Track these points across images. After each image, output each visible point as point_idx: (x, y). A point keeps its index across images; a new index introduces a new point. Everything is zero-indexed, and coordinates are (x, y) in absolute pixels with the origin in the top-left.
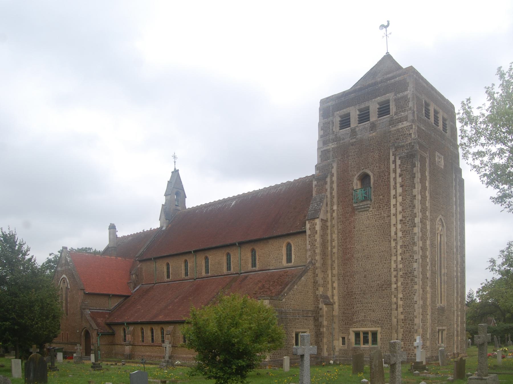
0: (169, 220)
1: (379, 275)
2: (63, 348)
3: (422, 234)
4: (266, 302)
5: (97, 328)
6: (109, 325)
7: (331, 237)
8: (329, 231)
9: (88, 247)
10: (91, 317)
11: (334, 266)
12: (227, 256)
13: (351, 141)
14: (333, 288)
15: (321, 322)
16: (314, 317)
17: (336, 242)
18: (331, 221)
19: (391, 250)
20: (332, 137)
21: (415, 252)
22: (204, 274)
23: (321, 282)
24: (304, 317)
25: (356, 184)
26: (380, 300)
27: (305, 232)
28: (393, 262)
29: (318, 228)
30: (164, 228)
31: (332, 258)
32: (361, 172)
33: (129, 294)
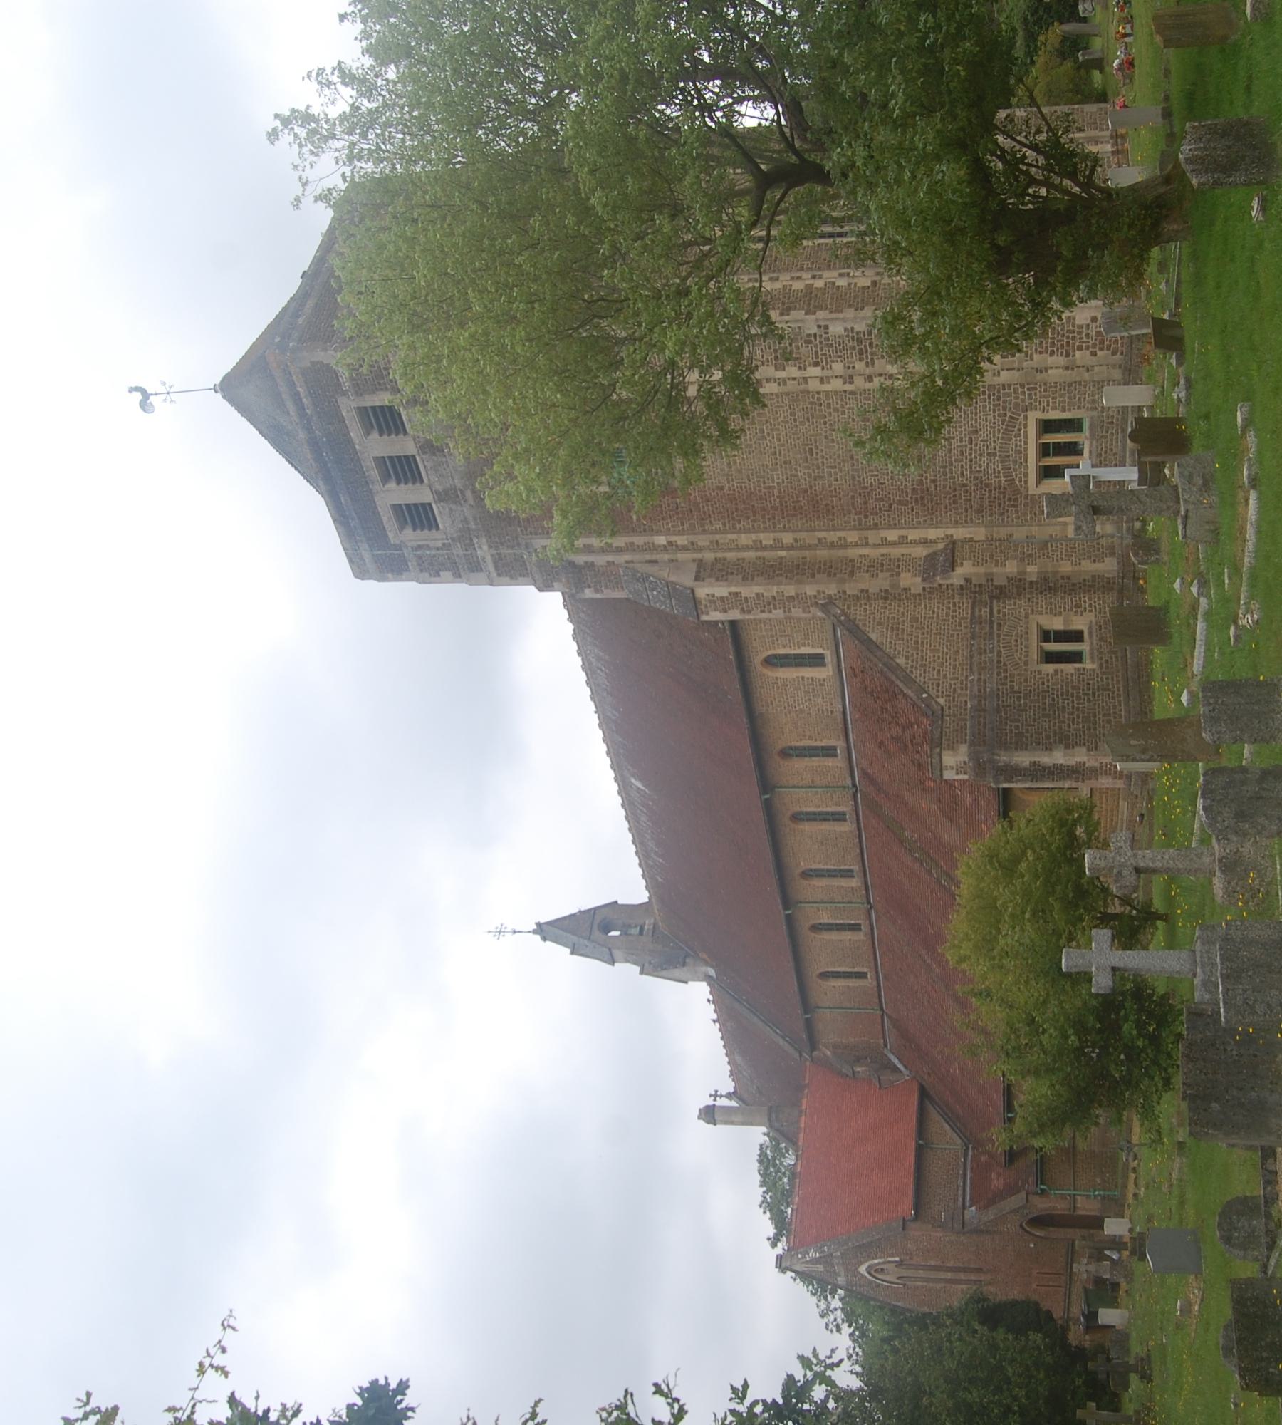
0: (687, 955)
2: (1086, 1290)
4: (949, 759)
5: (1023, 1194)
7: (747, 548)
8: (731, 556)
10: (986, 1207)
11: (835, 540)
13: (471, 501)
14: (902, 541)
15: (1009, 579)
17: (762, 536)
18: (701, 550)
19: (787, 394)
20: (458, 550)
22: (855, 883)
23: (881, 582)
24: (991, 634)
27: (733, 623)
28: (826, 387)
29: (721, 591)
30: (712, 972)
31: (809, 547)
33: (915, 1087)
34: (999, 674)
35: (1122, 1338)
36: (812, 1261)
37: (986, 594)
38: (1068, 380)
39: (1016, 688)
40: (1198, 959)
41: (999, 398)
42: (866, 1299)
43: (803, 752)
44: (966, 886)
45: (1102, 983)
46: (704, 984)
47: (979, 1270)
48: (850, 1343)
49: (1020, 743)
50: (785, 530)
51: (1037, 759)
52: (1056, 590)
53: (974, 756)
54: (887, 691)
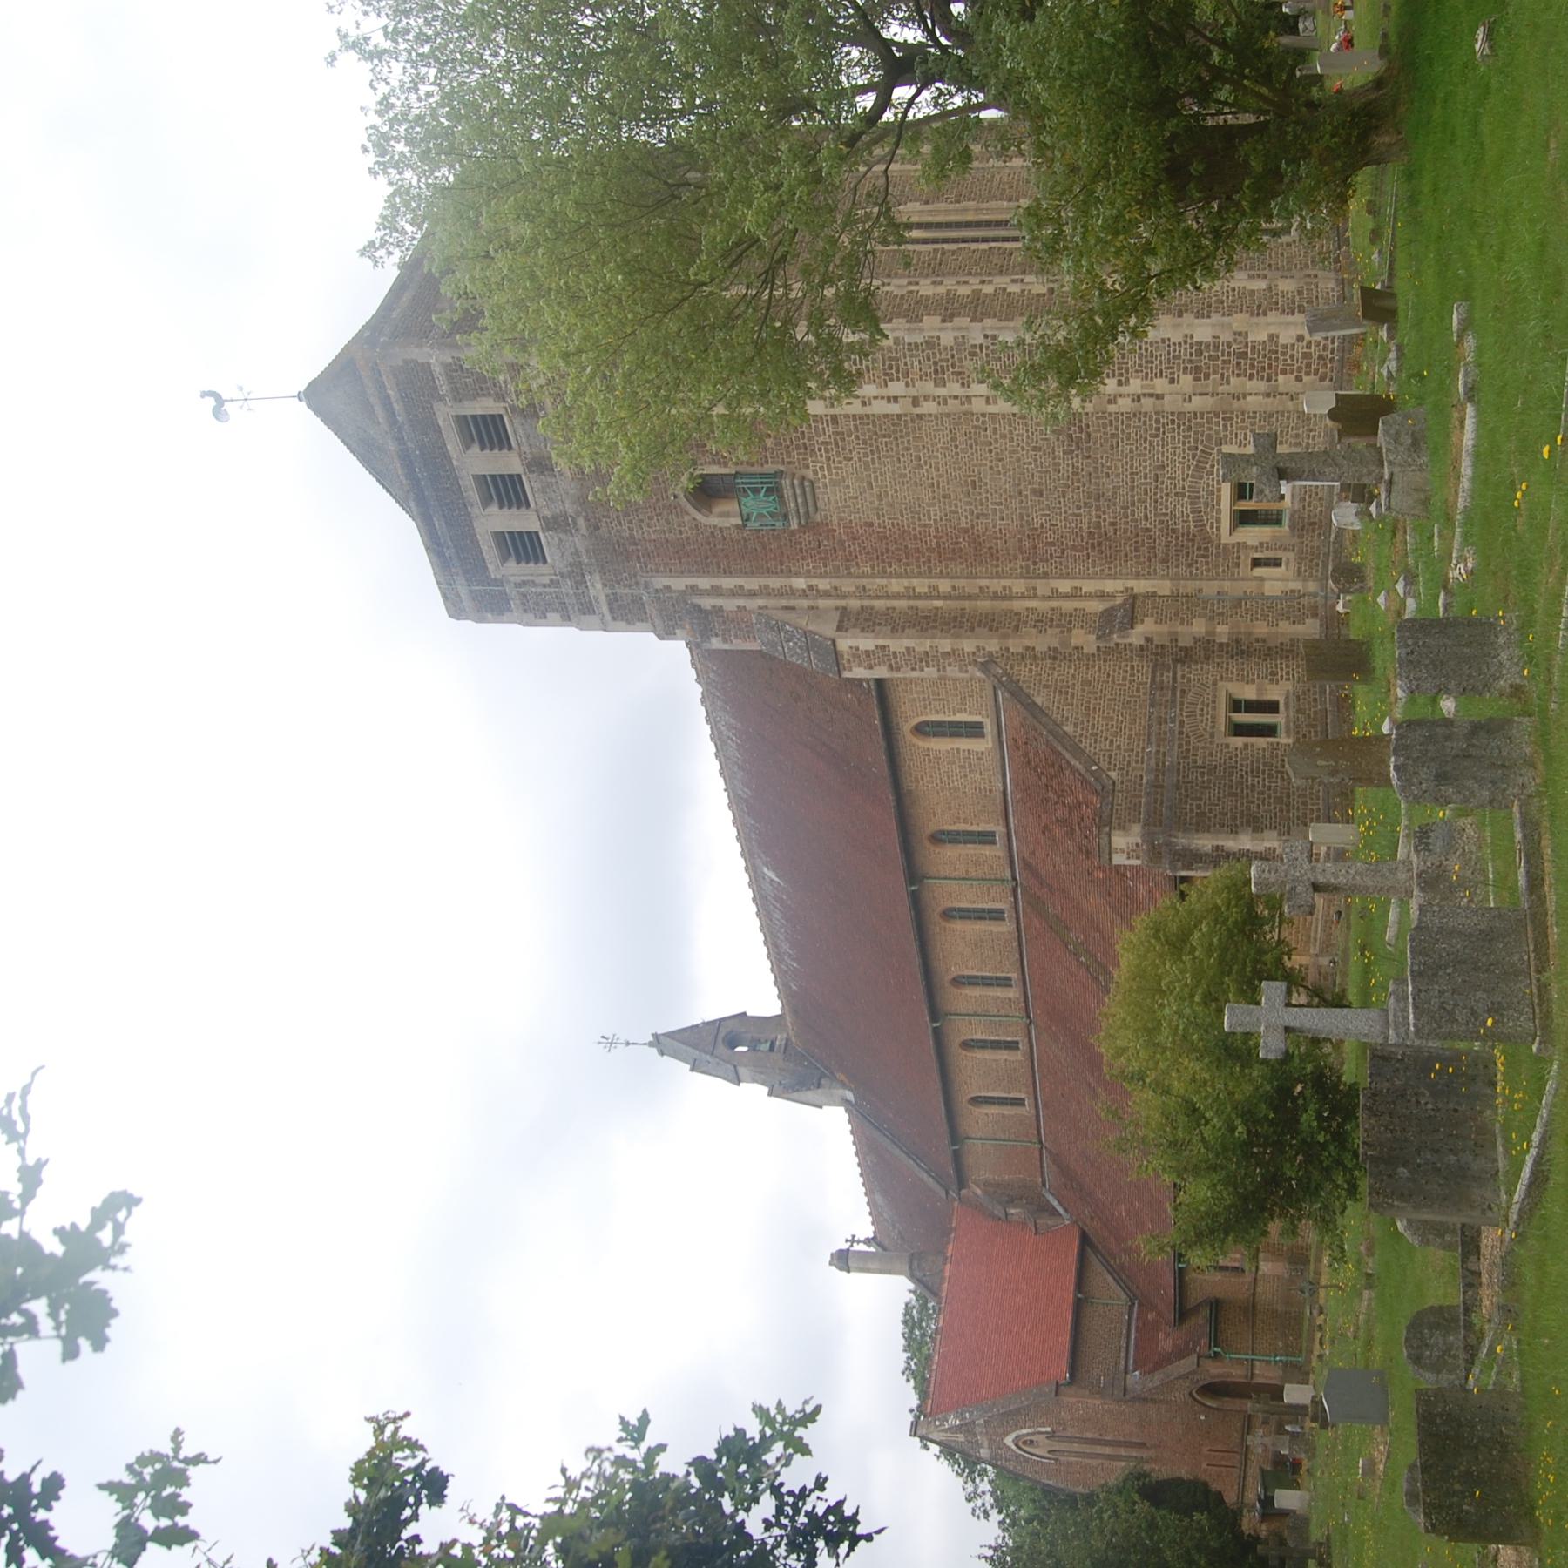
1: (1035, 449)
2: (1262, 1471)
3: (898, 316)
4: (1120, 841)
5: (1194, 1358)
6: (1183, 1313)
7: (897, 596)
9: (901, 1317)
10: (1152, 1371)
12: (954, 917)
13: (584, 531)
14: (1075, 594)
15: (1196, 640)
16: (1176, 661)
17: (915, 582)
18: (844, 596)
19: (948, 415)
20: (567, 588)
21: (960, 343)
22: (1013, 993)
24: (1173, 701)
25: (723, 517)
26: (1124, 447)
27: (880, 682)
28: (992, 409)
30: (850, 1096)
31: (970, 597)
32: (683, 501)
33: (1077, 1233)
34: (1180, 746)
35: (1300, 1522)
36: (950, 1429)
37: (1170, 657)
38: (1269, 409)
39: (1200, 763)
40: (1391, 1018)
41: (1190, 428)
42: (1016, 1477)
43: (956, 838)
44: (1124, 969)
45: (1270, 1047)
46: (842, 1109)
47: (1142, 1445)
48: (1000, 1532)
49: (1202, 824)
50: (941, 576)
51: (1220, 843)
52: (1249, 654)
53: (1148, 837)
54: (1053, 766)
